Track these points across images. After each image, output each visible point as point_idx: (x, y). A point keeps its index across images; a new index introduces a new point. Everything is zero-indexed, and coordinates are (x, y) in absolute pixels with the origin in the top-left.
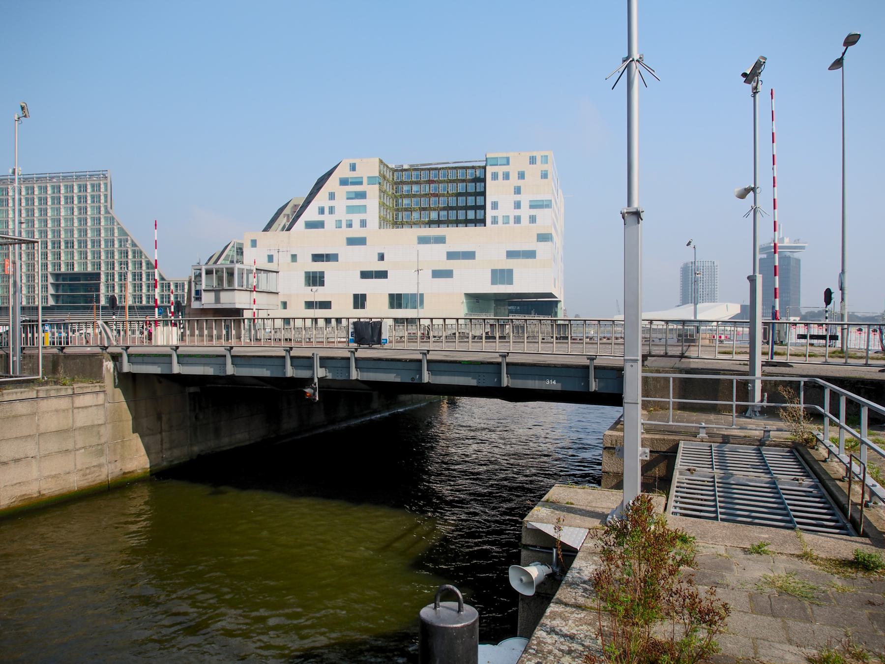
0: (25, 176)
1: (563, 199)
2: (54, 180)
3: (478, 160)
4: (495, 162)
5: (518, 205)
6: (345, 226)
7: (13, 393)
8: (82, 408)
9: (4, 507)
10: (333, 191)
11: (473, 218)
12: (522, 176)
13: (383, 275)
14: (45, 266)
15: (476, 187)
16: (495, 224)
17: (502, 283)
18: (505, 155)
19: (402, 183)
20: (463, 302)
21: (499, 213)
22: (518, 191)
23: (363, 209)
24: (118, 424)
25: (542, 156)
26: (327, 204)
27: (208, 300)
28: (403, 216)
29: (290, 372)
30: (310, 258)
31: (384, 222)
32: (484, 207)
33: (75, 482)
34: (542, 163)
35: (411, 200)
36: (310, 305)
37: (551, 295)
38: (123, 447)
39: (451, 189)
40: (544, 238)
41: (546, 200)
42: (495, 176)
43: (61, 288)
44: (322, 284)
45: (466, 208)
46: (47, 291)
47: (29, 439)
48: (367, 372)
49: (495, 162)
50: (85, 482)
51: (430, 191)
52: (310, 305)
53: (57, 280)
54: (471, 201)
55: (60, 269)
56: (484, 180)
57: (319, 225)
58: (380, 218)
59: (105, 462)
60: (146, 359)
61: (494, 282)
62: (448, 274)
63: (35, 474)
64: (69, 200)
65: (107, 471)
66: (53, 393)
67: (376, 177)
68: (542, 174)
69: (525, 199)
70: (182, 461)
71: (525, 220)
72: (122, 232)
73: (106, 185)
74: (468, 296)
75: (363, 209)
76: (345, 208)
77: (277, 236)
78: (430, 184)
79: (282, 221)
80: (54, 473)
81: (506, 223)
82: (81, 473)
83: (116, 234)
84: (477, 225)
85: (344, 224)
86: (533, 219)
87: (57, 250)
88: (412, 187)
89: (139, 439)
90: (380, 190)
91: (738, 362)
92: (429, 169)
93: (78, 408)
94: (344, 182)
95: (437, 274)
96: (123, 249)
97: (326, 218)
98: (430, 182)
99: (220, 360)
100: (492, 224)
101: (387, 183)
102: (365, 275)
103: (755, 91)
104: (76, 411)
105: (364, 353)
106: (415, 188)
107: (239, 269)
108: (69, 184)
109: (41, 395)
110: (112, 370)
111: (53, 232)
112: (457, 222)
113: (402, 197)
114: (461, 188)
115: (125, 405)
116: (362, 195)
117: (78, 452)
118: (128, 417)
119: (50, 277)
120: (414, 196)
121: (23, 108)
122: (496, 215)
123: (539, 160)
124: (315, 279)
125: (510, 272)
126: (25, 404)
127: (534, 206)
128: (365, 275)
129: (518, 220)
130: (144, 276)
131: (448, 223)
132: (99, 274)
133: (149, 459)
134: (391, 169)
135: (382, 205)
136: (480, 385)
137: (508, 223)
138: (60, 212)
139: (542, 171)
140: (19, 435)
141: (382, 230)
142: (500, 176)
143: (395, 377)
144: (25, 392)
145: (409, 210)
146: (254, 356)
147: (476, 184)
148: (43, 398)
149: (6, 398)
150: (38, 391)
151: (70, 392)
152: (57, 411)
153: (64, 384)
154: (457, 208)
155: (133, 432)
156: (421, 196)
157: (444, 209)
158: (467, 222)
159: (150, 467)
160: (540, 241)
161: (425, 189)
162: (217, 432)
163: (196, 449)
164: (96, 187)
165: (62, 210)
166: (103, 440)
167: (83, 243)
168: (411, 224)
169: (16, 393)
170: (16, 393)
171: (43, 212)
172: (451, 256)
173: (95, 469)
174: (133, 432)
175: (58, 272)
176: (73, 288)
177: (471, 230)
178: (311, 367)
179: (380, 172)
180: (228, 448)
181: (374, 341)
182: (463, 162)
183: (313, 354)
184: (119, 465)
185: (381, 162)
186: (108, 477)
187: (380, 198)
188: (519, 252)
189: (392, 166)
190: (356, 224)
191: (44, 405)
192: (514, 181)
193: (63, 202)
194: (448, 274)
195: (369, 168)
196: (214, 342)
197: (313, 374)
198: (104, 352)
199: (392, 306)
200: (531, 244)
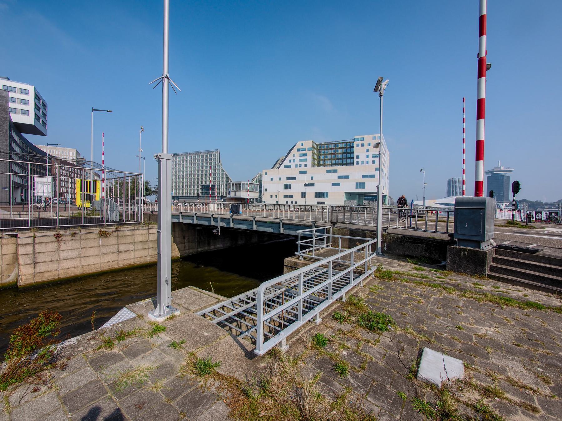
1: (389, 154)
4: (358, 140)
5: (367, 157)
13: (313, 185)
14: (198, 182)
18: (362, 136)
21: (359, 160)
22: (367, 151)
26: (292, 159)
27: (232, 194)
29: (213, 223)
30: (286, 179)
31: (313, 165)
32: (353, 158)
36: (286, 196)
39: (340, 151)
42: (358, 145)
43: (203, 190)
44: (290, 188)
45: (346, 158)
47: (131, 244)
49: (358, 140)
52: (286, 196)
54: (348, 156)
56: (353, 147)
57: (289, 166)
61: (357, 188)
62: (338, 184)
63: (132, 256)
64: (206, 160)
66: (140, 228)
71: (370, 162)
72: (223, 171)
73: (218, 154)
74: (346, 193)
75: (306, 160)
77: (275, 170)
79: (278, 165)
80: (140, 256)
82: (151, 257)
83: (221, 171)
85: (298, 166)
89: (176, 245)
92: (332, 144)
94: (299, 150)
95: (334, 184)
96: (223, 176)
97: (293, 164)
98: (332, 149)
102: (307, 185)
103: (381, 95)
104: (149, 234)
106: (326, 151)
109: (136, 228)
111: (201, 171)
112: (343, 164)
113: (321, 155)
114: (344, 150)
116: (305, 155)
117: (150, 249)
119: (200, 186)
120: (326, 154)
121: (142, 128)
124: (287, 187)
125: (364, 183)
126: (130, 232)
129: (367, 162)
131: (339, 164)
134: (317, 144)
135: (313, 158)
137: (363, 164)
145: (324, 160)
148: (137, 230)
149: (122, 229)
150: (134, 227)
151: (147, 228)
152: (142, 234)
154: (342, 159)
156: (328, 154)
157: (337, 159)
158: (347, 164)
161: (332, 151)
162: (209, 244)
163: (199, 250)
165: (204, 163)
168: (324, 165)
171: (198, 164)
172: (339, 177)
177: (348, 167)
178: (217, 222)
180: (214, 250)
185: (313, 142)
188: (342, 176)
191: (137, 232)
192: (366, 147)
194: (338, 184)
195: (308, 144)
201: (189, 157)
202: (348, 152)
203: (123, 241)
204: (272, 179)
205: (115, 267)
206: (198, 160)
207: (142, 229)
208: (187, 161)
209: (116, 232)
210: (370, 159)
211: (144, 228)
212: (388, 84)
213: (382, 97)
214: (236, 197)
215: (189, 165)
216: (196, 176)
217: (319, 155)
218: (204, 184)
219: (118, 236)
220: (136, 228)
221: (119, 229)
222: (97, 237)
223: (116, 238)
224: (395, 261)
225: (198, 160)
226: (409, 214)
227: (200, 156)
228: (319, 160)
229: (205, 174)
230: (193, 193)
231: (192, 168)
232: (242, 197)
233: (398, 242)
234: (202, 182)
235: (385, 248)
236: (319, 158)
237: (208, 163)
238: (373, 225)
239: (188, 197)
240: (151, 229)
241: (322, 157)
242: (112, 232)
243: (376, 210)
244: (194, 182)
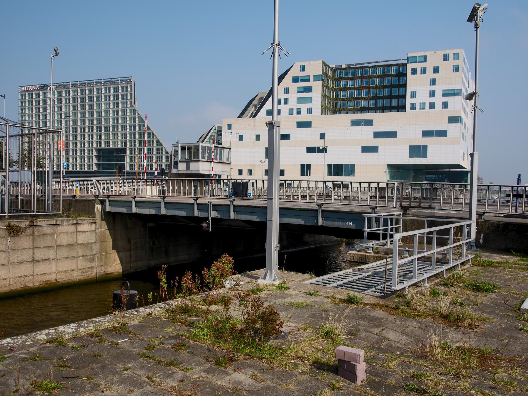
0: (80, 82)
2: (99, 84)
3: (402, 59)
4: (414, 60)
5: (433, 94)
6: (296, 113)
7: (42, 221)
8: (82, 232)
9: (36, 287)
10: (287, 87)
11: (381, 106)
12: (436, 70)
13: (324, 150)
14: (91, 144)
15: (399, 80)
16: (413, 109)
17: (418, 156)
18: (423, 54)
19: (341, 79)
20: (386, 172)
21: (417, 101)
22: (433, 82)
23: (309, 100)
24: (103, 243)
25: (454, 54)
27: (182, 167)
28: (341, 105)
29: (196, 213)
31: (325, 110)
32: (404, 97)
33: (77, 276)
34: (454, 59)
35: (347, 92)
37: (459, 167)
38: (106, 257)
39: (378, 82)
40: (454, 120)
41: (456, 90)
42: (414, 72)
45: (391, 97)
46: (93, 161)
47: (51, 249)
48: (241, 214)
49: (414, 60)
50: (82, 277)
51: (362, 84)
53: (99, 153)
54: (394, 91)
55: (101, 146)
56: (405, 75)
58: (322, 106)
59: (95, 266)
60: (119, 204)
61: (411, 156)
63: (54, 269)
64: (107, 98)
65: (96, 272)
66: (65, 222)
67: (320, 75)
68: (454, 68)
69: (439, 89)
70: (143, 270)
73: (131, 86)
74: (390, 166)
75: (309, 100)
76: (296, 99)
77: (247, 120)
78: (362, 79)
79: (252, 110)
80: (64, 270)
81: (422, 109)
83: (137, 122)
84: (384, 111)
85: (295, 112)
86: (445, 105)
87: (99, 133)
88: (348, 82)
90: (323, 85)
91: (494, 215)
92: (362, 68)
93: (80, 232)
94: (296, 80)
95: (366, 149)
98: (362, 77)
99: (158, 204)
100: (411, 109)
101: (328, 80)
102: (310, 150)
103: (477, 26)
104: (78, 234)
105: (238, 202)
106: (350, 83)
107: (202, 146)
108: (108, 87)
109: (58, 223)
110: (100, 210)
111: (97, 120)
112: (383, 109)
113: (341, 90)
114: (386, 81)
115: (108, 232)
116: (309, 89)
117: (79, 259)
118: (109, 240)
120: (350, 89)
121: (55, 50)
122: (414, 102)
123: (451, 57)
125: (425, 148)
126: (49, 228)
127: (446, 94)
128: (310, 150)
129: (432, 106)
130: (155, 151)
131: (376, 109)
132: (126, 149)
133: (122, 266)
135: (324, 96)
136: (306, 224)
137: (424, 108)
138: (102, 106)
139: (454, 66)
140: (45, 245)
141: (324, 116)
142: (419, 71)
143: (257, 218)
144: (49, 220)
145: (345, 99)
146: (177, 203)
147: (399, 78)
148: (59, 225)
149: (39, 223)
150: (56, 221)
151: (75, 222)
152: (67, 233)
153: (72, 217)
154: (383, 98)
155: (113, 249)
156: (355, 89)
157: (372, 98)
158: (391, 109)
159: (123, 272)
160: (451, 123)
161: (362, 83)
164: (125, 89)
165: (103, 105)
166: (94, 252)
167: (115, 128)
168: (347, 111)
169: (44, 221)
170: (44, 221)
172: (377, 135)
173: (89, 270)
174: (113, 249)
175: (100, 148)
176: (109, 159)
178: (207, 211)
179: (323, 71)
180: (174, 264)
181: (243, 194)
182: (389, 61)
183: (209, 202)
184: (103, 268)
185: (324, 63)
186: (96, 275)
187: (323, 91)
188: (383, 133)
189: (333, 66)
190: (304, 111)
191: (60, 229)
192: (430, 74)
193: (103, 100)
194: (374, 149)
196: (170, 194)
197: (209, 215)
198: (96, 199)
199: (330, 174)
200: (444, 125)
201: (71, 92)
202: (394, 83)
203: (40, 243)
204: (241, 138)
205: (30, 285)
206: (91, 98)
207: (67, 225)
208: (67, 100)
209: (31, 228)
210: (439, 100)
211: (71, 222)
212: (486, 9)
213: (478, 29)
214: (189, 172)
215: (71, 107)
216: (87, 131)
217: (335, 90)
218: (103, 146)
219: (33, 235)
220: (58, 223)
221: (35, 224)
222: (4, 235)
223: (31, 237)
224: (495, 255)
225: (91, 98)
226: (515, 193)
227: (95, 90)
228: (336, 100)
229: (105, 128)
230: (81, 165)
231: (79, 114)
232: (201, 172)
233: (499, 231)
234: (99, 143)
235: (481, 241)
236: (336, 96)
237: (112, 105)
238: (463, 210)
239: (78, 173)
240: (80, 224)
241: (343, 93)
242: (26, 227)
243: (469, 187)
244: (83, 144)
